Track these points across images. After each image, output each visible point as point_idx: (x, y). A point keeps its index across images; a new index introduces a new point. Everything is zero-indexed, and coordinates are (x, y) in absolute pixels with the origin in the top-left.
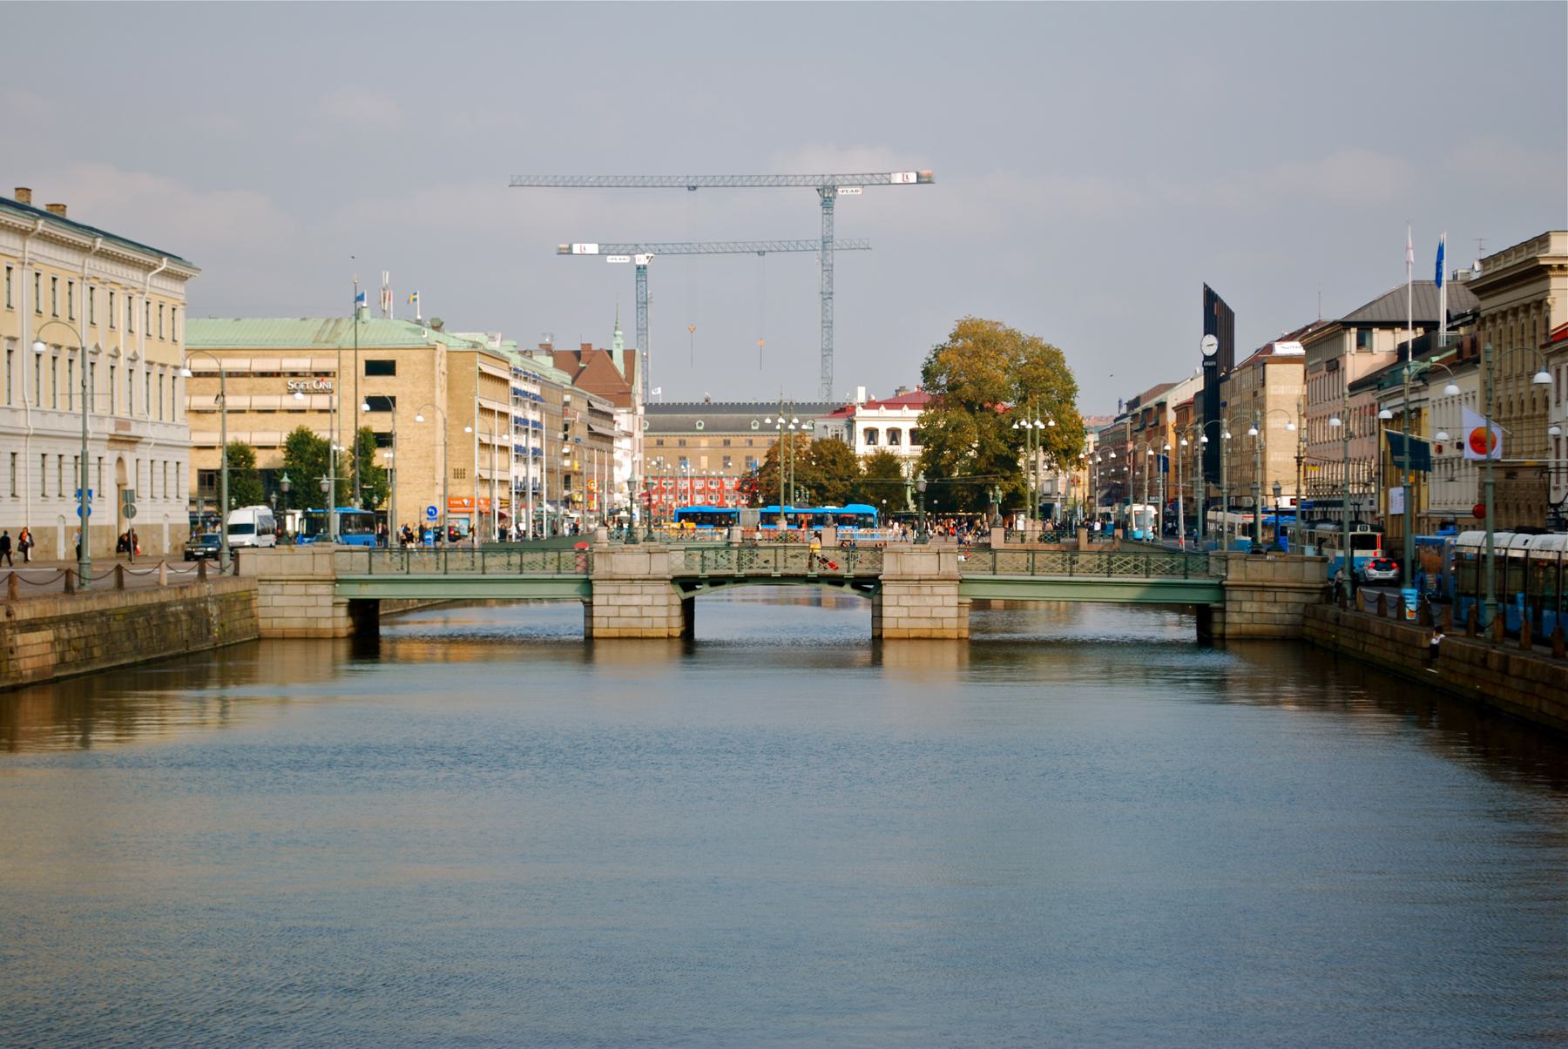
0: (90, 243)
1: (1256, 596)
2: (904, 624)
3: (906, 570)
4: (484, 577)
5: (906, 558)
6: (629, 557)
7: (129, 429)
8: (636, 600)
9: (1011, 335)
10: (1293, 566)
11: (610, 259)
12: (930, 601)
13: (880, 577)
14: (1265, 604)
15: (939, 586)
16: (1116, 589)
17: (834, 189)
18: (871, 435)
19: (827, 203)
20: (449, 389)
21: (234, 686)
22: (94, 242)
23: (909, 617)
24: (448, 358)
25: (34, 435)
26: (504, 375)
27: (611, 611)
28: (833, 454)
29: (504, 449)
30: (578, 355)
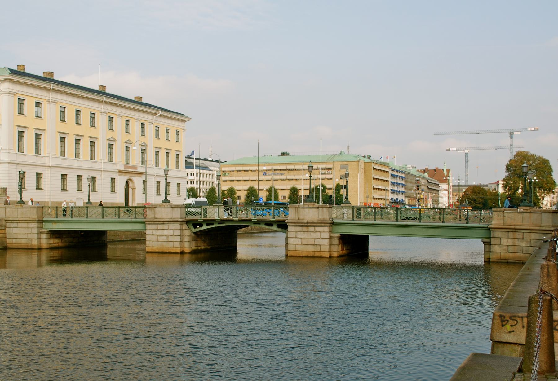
0: (102, 99)
1: (511, 235)
2: (299, 248)
4: (119, 220)
5: (301, 210)
6: (163, 209)
7: (137, 169)
8: (166, 232)
9: (533, 156)
10: (535, 216)
11: (459, 151)
12: (313, 235)
13: (286, 221)
14: (516, 240)
15: (319, 226)
16: (424, 229)
17: (513, 132)
19: (511, 136)
20: (365, 173)
22: (103, 99)
23: (302, 244)
24: (364, 164)
25: (103, 171)
26: (388, 170)
27: (154, 238)
28: (478, 191)
29: (388, 190)
30: (435, 170)
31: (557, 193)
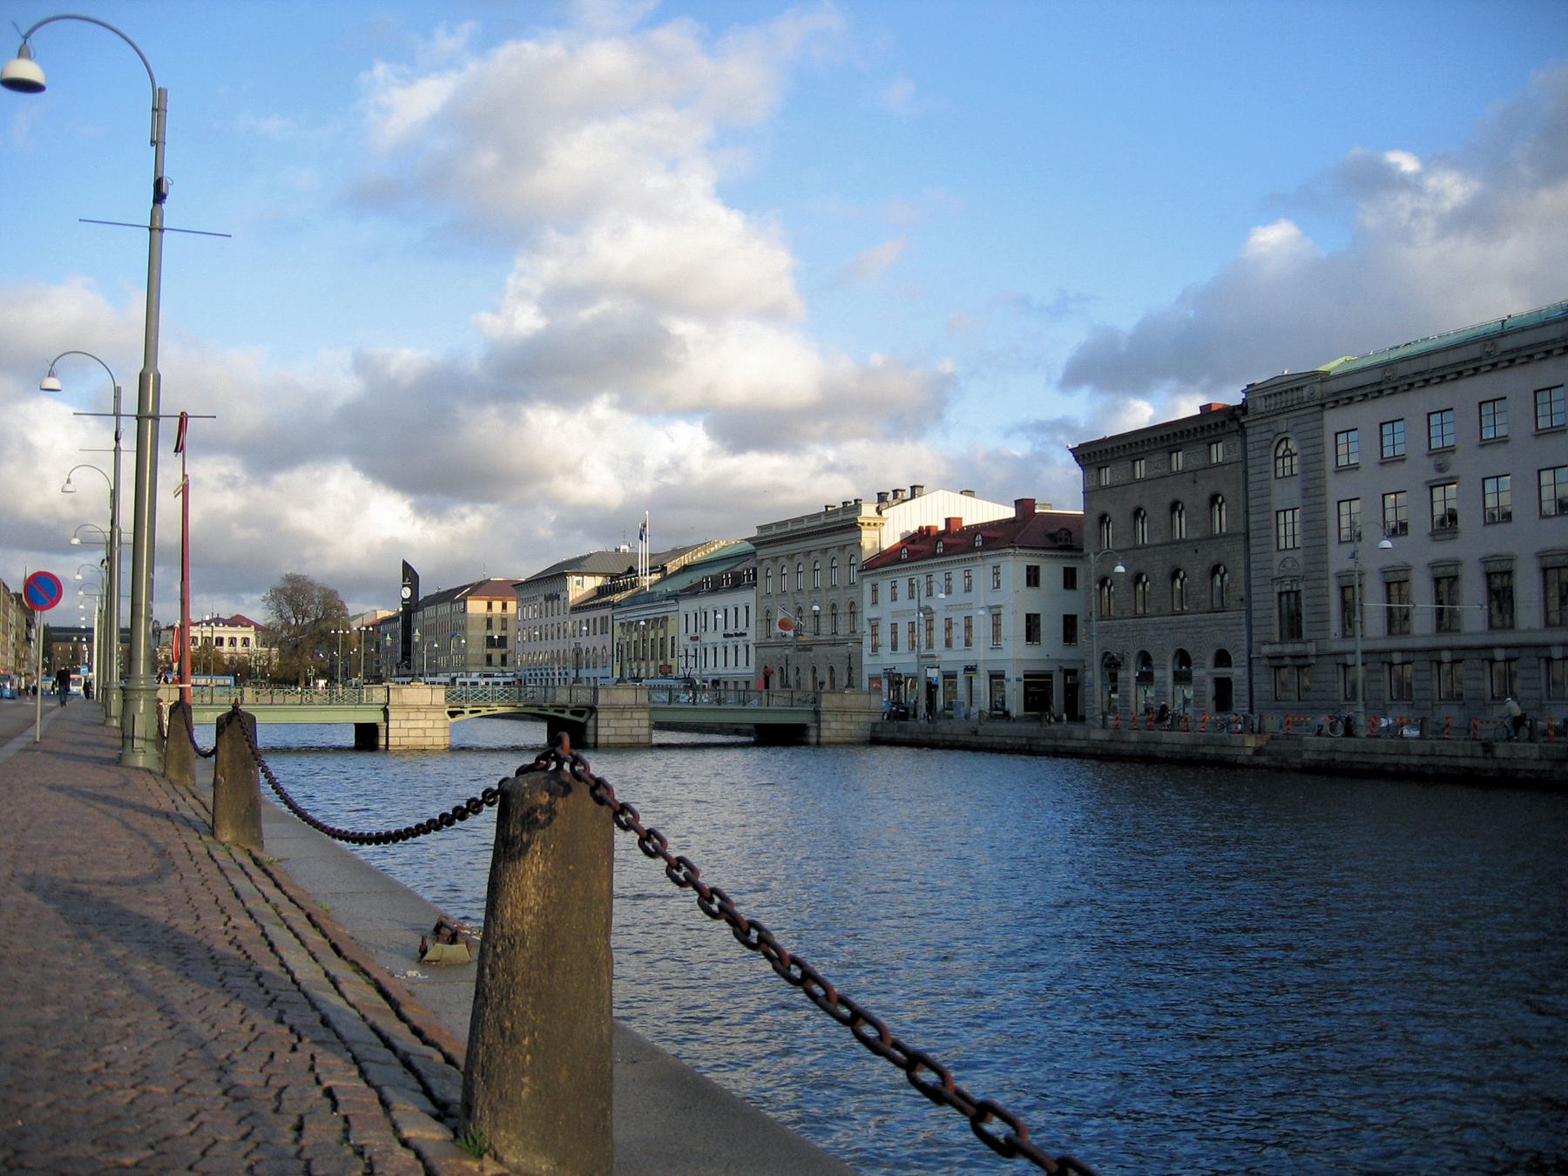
3: (615, 701)
8: (421, 724)
18: (233, 641)
21: (411, 506)
23: (616, 735)
27: (403, 733)
31: (482, 1169)
